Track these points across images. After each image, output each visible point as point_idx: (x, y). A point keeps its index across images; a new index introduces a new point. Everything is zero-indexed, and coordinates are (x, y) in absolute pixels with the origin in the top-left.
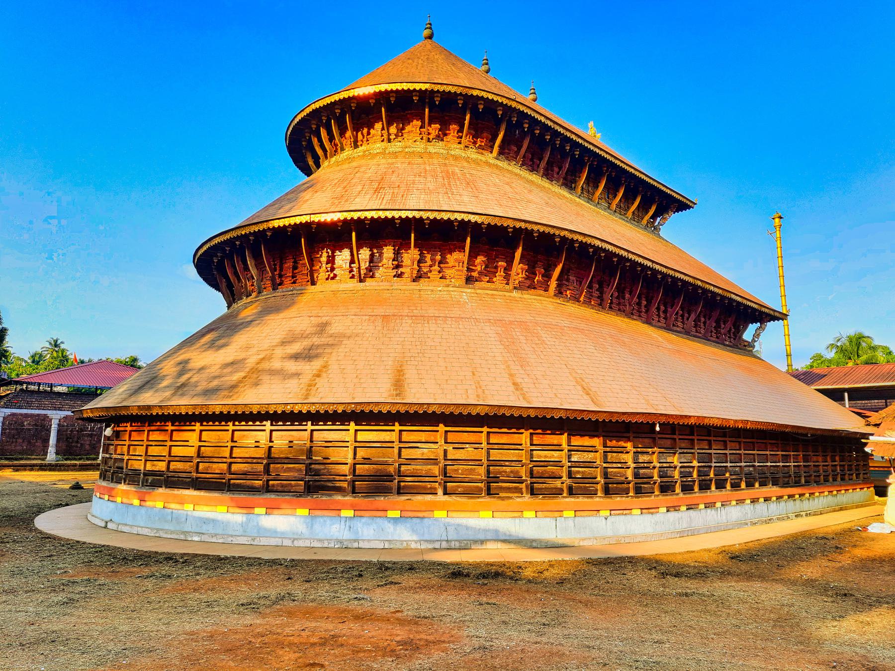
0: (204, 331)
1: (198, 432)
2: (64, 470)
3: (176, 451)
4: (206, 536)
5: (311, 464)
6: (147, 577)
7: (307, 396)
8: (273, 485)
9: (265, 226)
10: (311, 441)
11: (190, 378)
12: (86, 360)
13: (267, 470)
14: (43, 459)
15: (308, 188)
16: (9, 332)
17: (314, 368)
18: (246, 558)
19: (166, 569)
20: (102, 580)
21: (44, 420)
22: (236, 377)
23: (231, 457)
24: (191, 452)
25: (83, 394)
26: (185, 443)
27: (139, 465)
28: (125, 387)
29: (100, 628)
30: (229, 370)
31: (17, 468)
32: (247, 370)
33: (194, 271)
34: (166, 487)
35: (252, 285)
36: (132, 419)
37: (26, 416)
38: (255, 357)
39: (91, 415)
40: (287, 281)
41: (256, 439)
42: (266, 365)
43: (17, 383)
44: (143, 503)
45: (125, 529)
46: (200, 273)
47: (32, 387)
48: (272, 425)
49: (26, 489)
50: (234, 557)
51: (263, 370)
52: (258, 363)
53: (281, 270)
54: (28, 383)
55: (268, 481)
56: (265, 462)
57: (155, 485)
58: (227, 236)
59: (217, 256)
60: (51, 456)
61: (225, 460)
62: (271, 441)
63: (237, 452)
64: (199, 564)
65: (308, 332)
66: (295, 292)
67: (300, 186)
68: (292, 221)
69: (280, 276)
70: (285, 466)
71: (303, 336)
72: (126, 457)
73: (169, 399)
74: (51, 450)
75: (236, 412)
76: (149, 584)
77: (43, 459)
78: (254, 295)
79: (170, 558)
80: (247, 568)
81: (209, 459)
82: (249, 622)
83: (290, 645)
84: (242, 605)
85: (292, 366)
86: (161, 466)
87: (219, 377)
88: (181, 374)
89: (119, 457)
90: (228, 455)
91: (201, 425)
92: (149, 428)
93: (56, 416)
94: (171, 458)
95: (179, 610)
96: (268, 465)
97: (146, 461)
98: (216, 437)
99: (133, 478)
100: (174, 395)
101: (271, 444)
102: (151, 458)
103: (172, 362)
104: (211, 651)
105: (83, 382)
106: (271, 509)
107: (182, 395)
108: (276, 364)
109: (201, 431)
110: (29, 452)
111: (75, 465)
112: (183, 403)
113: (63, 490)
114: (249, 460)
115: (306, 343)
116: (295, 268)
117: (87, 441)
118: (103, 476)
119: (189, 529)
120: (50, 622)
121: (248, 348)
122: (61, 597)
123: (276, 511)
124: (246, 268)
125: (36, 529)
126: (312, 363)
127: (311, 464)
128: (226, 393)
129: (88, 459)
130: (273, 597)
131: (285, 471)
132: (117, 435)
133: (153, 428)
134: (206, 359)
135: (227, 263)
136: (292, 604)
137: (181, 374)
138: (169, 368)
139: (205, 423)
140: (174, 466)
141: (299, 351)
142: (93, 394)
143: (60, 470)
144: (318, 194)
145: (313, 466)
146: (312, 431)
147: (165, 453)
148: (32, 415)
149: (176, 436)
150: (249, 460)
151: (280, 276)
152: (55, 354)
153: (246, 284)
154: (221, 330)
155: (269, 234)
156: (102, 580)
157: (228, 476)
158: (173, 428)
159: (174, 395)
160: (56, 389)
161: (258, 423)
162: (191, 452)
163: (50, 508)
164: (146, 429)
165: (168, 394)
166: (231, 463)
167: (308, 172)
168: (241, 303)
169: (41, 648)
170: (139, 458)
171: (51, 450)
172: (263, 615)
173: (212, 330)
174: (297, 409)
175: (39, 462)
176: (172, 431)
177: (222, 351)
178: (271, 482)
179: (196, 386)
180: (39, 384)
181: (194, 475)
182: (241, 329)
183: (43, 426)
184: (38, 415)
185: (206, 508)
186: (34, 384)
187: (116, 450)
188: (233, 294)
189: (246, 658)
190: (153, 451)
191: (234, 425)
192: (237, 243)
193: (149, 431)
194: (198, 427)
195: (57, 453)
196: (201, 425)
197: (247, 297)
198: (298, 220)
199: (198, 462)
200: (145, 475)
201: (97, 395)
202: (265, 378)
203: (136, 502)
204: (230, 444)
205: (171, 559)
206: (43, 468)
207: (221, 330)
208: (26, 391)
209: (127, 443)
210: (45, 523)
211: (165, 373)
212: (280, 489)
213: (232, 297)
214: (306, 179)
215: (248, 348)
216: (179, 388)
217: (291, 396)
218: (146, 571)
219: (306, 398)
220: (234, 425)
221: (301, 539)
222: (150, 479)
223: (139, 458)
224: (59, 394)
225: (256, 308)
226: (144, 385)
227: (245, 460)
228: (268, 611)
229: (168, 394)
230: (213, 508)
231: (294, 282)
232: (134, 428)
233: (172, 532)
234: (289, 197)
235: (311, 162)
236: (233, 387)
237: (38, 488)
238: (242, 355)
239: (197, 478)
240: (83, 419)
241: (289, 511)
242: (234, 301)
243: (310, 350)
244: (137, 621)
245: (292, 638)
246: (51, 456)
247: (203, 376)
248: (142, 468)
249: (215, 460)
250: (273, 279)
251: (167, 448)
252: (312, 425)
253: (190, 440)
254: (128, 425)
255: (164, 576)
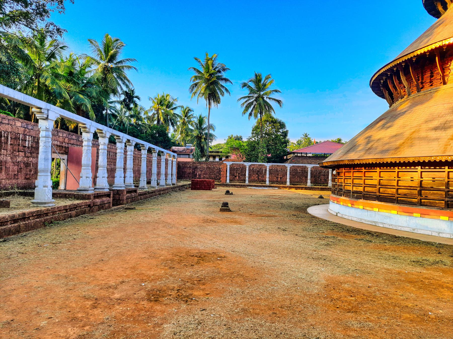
0: (378, 120)
1: (378, 172)
2: (315, 190)
3: (367, 182)
4: (386, 225)
5: (448, 191)
6: (360, 240)
7: (445, 151)
8: (424, 202)
9: (412, 55)
10: (448, 178)
11: (372, 145)
12: (319, 142)
13: (420, 194)
14: (306, 185)
15: (440, 25)
16: (289, 132)
17: (448, 134)
18: (411, 239)
19: (368, 237)
20: (339, 238)
21: (305, 168)
22: (398, 143)
23: (398, 186)
24: (375, 182)
25: (319, 157)
26: (371, 178)
27: (350, 188)
28: (341, 152)
29: (343, 258)
30: (394, 139)
31: (297, 188)
32: (405, 139)
33: (371, 89)
34: (364, 199)
35: (404, 92)
36: (345, 166)
37: (298, 167)
38: (409, 131)
39: (327, 165)
40: (427, 85)
41: (411, 177)
42: (416, 135)
43: (294, 153)
44: (353, 206)
45: (345, 217)
46: (373, 90)
47: (299, 155)
48: (421, 168)
49: (301, 197)
50: (404, 237)
51: (415, 138)
52: (411, 135)
53: (422, 79)
54: (297, 153)
55: (421, 199)
56: (418, 189)
57: (358, 198)
58: (389, 67)
59: (383, 79)
60: (309, 184)
61: (394, 187)
62: (421, 178)
63: (400, 183)
64: (385, 238)
65: (442, 114)
66: (431, 91)
67: (433, 25)
68: (429, 48)
69: (422, 83)
70: (431, 192)
71: (439, 116)
72: (343, 184)
73: (363, 156)
74: (309, 181)
75: (400, 162)
76: (362, 243)
77: (306, 185)
78: (405, 97)
79: (369, 233)
80: (412, 244)
81: (385, 186)
82: (419, 271)
83: (447, 287)
84: (414, 261)
85: (433, 134)
86: (361, 189)
87: (388, 143)
88: (368, 143)
89: (340, 184)
90: (396, 185)
91: (380, 169)
92: (353, 171)
93: (309, 167)
94: (366, 185)
95: (379, 257)
96: (420, 191)
97: (353, 186)
98: (388, 176)
99: (347, 193)
100: (365, 153)
101: (422, 179)
102: (355, 185)
103: (363, 138)
104: (400, 280)
105: (319, 152)
106: (423, 215)
107: (369, 154)
108: (423, 134)
109: (380, 172)
110: (300, 182)
111: (318, 188)
112: (370, 158)
113: (315, 198)
114: (409, 188)
115: (442, 120)
116: (432, 76)
117: (322, 177)
118: (333, 193)
119: (377, 221)
120: (321, 251)
121: (404, 127)
122: (323, 242)
123: (426, 216)
124: (401, 82)
125: (308, 213)
126: (447, 132)
127: (448, 191)
128: (393, 152)
129: (324, 186)
130: (432, 261)
131: (431, 194)
132: (338, 174)
133: (355, 170)
134: (382, 135)
135: (386, 84)
136: (444, 267)
137: (368, 143)
138: (361, 141)
139: (382, 168)
140: (367, 189)
141: (437, 125)
142: (324, 157)
143: (313, 190)
144: (447, 26)
145: (450, 193)
146: (449, 172)
147: (362, 183)
148: (300, 167)
149: (367, 174)
150: (409, 188)
151: (422, 83)
152: (306, 140)
153: (400, 92)
154: (387, 119)
155: (414, 59)
156: (339, 238)
157: (397, 196)
158: (365, 170)
159: (365, 153)
160: (308, 155)
161: (413, 168)
162: (375, 182)
163: (312, 205)
164: (352, 171)
165: (362, 153)
166: (398, 189)
167: (437, 15)
168: (397, 103)
169: (321, 261)
170: (350, 185)
171: (309, 181)
172: (427, 269)
173: (383, 119)
174: (438, 159)
175: (304, 186)
176: (365, 172)
177: (389, 130)
178: (423, 200)
179: (376, 149)
180: (302, 153)
181: (378, 194)
182: (399, 117)
183: (305, 171)
184: (303, 166)
185: (385, 211)
186: (299, 153)
187: (338, 181)
188: (392, 98)
189: (420, 288)
190: (356, 181)
191: (398, 169)
192: (395, 69)
193: (353, 172)
194: (378, 170)
195: (311, 183)
196: (380, 169)
197: (402, 98)
198: (433, 47)
199: (380, 188)
200: (353, 193)
201: (327, 157)
202: (417, 142)
203: (350, 205)
204: (396, 179)
205: (370, 233)
206: (306, 188)
207: (387, 119)
208: (297, 156)
209: (343, 178)
210: (312, 210)
211: (360, 144)
212: (429, 204)
213: (392, 100)
214: (436, 20)
215: (404, 127)
216: (367, 150)
217: (433, 152)
218: (359, 237)
219: (444, 153)
220: (398, 169)
221: (444, 233)
222: (356, 195)
223: (350, 185)
224: (310, 157)
225: (407, 104)
226: (349, 150)
227: (406, 188)
228: (429, 267)
229: (362, 153)
230: (389, 211)
231: (432, 85)
232: (346, 171)
233: (368, 221)
234: (426, 34)
235: (440, 8)
236: (397, 148)
237: (306, 197)
238: (401, 131)
239: (379, 196)
240: (323, 167)
241: (436, 217)
242: (393, 102)
243: (445, 124)
244: (359, 259)
245: (448, 284)
246: (309, 184)
247: (380, 143)
248: (351, 189)
249: (389, 187)
250: (417, 86)
251: (363, 180)
252: (449, 168)
253: (374, 177)
254: (343, 169)
255: (368, 241)
